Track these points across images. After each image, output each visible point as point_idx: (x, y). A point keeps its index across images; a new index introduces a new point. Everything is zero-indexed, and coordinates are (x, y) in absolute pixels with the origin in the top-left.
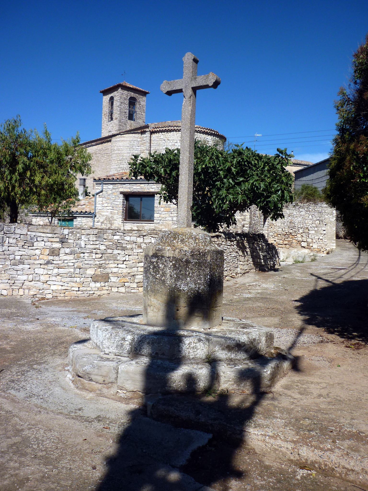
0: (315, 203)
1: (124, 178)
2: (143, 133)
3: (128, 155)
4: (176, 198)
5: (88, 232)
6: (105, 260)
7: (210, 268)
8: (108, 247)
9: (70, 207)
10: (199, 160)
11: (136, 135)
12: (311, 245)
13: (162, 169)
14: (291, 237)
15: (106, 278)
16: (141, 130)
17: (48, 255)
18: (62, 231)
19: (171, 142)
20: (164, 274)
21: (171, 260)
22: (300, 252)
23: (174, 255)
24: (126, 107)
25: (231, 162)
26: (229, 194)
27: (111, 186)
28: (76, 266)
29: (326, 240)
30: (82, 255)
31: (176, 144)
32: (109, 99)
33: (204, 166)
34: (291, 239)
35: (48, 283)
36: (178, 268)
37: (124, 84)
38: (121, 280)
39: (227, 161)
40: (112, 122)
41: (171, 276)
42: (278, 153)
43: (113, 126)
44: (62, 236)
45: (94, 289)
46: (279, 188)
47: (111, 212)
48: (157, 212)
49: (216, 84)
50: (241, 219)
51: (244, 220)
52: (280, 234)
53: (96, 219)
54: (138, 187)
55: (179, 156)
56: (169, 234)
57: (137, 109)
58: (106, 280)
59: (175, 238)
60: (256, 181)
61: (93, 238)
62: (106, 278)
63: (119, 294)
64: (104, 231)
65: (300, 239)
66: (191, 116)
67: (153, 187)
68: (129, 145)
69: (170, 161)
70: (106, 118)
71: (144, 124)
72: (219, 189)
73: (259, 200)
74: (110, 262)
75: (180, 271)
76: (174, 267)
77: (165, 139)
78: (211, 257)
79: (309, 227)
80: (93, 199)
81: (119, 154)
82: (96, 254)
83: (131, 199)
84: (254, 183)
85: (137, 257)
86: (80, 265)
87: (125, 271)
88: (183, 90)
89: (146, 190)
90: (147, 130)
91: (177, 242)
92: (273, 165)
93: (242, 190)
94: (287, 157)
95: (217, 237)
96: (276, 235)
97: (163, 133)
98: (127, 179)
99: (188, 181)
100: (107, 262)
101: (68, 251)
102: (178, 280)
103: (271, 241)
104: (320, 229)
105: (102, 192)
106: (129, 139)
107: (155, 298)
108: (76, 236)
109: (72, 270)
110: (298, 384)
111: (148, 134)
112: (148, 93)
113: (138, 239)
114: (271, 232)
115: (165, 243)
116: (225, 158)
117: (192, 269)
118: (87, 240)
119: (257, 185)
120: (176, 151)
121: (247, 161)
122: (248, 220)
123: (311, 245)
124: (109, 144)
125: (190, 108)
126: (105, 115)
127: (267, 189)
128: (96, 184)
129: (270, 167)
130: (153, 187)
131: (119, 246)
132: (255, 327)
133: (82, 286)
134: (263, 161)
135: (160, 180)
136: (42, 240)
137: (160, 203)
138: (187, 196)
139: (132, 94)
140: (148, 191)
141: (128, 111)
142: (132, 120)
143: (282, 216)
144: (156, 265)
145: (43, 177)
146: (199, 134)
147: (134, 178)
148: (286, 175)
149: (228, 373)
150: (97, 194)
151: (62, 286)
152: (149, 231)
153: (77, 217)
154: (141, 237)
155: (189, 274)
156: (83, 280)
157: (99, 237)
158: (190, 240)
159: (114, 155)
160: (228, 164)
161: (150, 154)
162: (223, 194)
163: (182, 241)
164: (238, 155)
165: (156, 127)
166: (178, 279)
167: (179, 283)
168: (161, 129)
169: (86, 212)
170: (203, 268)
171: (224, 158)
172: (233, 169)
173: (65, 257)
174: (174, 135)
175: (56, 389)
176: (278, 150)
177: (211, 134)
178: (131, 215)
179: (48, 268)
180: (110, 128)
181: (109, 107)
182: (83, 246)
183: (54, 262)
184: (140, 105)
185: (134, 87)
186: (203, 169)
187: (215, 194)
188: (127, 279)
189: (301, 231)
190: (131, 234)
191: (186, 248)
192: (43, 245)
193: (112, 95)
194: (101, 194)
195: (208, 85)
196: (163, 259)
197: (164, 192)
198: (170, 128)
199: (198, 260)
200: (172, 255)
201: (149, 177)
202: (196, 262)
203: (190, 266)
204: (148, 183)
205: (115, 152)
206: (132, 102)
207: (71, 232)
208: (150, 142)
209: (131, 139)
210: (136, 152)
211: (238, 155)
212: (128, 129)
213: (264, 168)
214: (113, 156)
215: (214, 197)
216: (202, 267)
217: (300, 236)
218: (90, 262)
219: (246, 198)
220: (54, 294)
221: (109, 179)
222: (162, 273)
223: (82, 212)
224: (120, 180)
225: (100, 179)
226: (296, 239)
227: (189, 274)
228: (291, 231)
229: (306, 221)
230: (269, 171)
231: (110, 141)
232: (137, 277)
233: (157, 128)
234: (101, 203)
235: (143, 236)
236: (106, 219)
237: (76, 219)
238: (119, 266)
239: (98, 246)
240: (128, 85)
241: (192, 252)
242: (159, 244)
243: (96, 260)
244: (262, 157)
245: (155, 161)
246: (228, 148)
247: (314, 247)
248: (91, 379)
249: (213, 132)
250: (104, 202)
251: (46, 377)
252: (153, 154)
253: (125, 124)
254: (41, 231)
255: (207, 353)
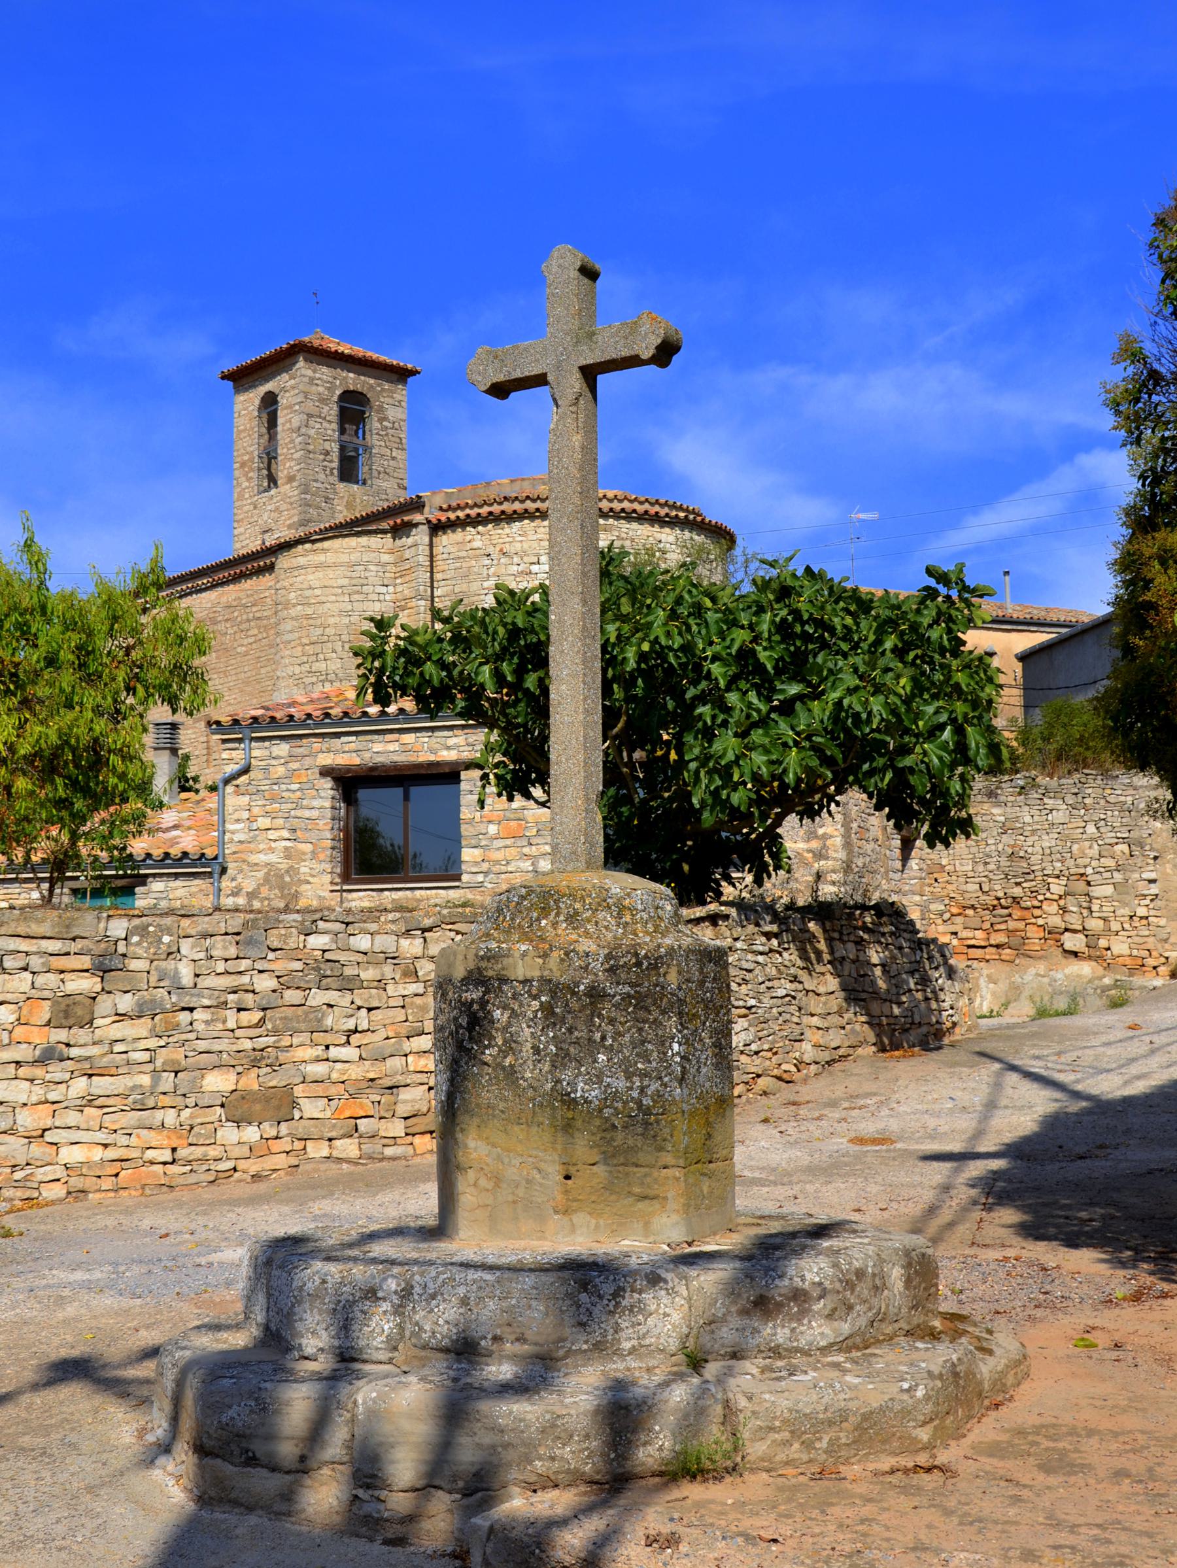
0: (1106, 774)
1: (336, 712)
2: (400, 531)
3: (346, 620)
4: (543, 779)
5: (204, 924)
6: (276, 1032)
7: (680, 1014)
8: (285, 982)
9: (124, 835)
10: (626, 628)
11: (374, 541)
12: (1103, 943)
13: (486, 669)
14: (1017, 914)
15: (281, 1106)
16: (395, 520)
17: (48, 1024)
18: (102, 925)
19: (516, 560)
20: (511, 1045)
21: (534, 991)
22: (1059, 976)
23: (546, 973)
24: (327, 431)
25: (751, 627)
26: (750, 750)
27: (282, 749)
28: (159, 1063)
29: (1163, 922)
30: (184, 1017)
31: (535, 568)
32: (257, 402)
33: (646, 647)
34: (1021, 925)
35: (49, 1137)
36: (563, 1021)
37: (316, 343)
38: (342, 1111)
39: (735, 624)
40: (273, 492)
41: (536, 1050)
42: (932, 582)
43: (277, 509)
44: (103, 945)
45: (236, 1152)
46: (943, 718)
47: (286, 848)
48: (473, 842)
49: (666, 352)
50: (809, 851)
51: (820, 855)
52: (973, 907)
53: (226, 883)
54: (392, 747)
55: (546, 614)
56: (523, 898)
57: (374, 440)
58: (282, 1114)
59: (545, 912)
60: (851, 691)
61: (223, 948)
62: (281, 1106)
63: (334, 1166)
64: (267, 919)
65: (1056, 921)
66: (581, 469)
67: (451, 742)
68: (345, 582)
69: (514, 633)
70: (249, 479)
71: (403, 497)
72: (709, 735)
73: (866, 767)
74: (296, 1041)
75: (570, 1030)
76: (546, 1018)
77: (490, 550)
78: (679, 973)
79: (1089, 871)
80: (212, 802)
81: (308, 617)
82: (239, 1010)
83: (363, 794)
84: (846, 702)
85: (400, 1015)
86: (175, 1056)
87: (355, 1072)
88: (550, 378)
89: (424, 757)
90: (417, 518)
91: (555, 925)
92: (914, 627)
93: (798, 734)
94: (966, 595)
95: (713, 919)
96: (955, 910)
97: (480, 528)
98: (346, 714)
99: (585, 700)
100: (286, 1041)
101: (126, 1003)
102: (564, 1065)
103: (927, 930)
104: (1136, 876)
105: (246, 770)
106: (344, 558)
107: (480, 1138)
108: (160, 941)
109: (145, 1080)
110: (1038, 1439)
111: (421, 535)
112: (414, 373)
113: (405, 943)
114: (936, 899)
115: (507, 932)
116: (728, 611)
117: (612, 1021)
118: (202, 955)
119: (858, 708)
120: (536, 597)
121: (811, 618)
122: (838, 853)
123: (1103, 943)
124: (266, 580)
125: (577, 439)
126: (243, 465)
127: (900, 720)
128: (224, 741)
129: (902, 640)
130: (455, 743)
131: (328, 972)
132: (863, 1231)
133: (185, 1142)
134: (876, 618)
135: (476, 713)
136: (21, 964)
137: (482, 803)
138: (581, 757)
139: (352, 380)
140: (432, 758)
141: (335, 447)
142: (357, 483)
143: (966, 826)
144: (481, 1014)
145: (22, 726)
146: (623, 524)
147: (374, 710)
148: (967, 666)
149: (767, 1396)
150: (227, 781)
151: (106, 1146)
152: (445, 912)
153: (147, 876)
154: (414, 937)
155: (603, 1038)
156: (191, 1117)
157: (250, 942)
158: (601, 915)
159: (289, 625)
160: (741, 636)
161: (436, 614)
162: (725, 750)
163: (573, 919)
164: (778, 600)
165: (454, 504)
166: (561, 1059)
167: (566, 1076)
168: (473, 512)
169: (185, 854)
170: (655, 1014)
171: (724, 612)
172: (763, 656)
173: (117, 1031)
174: (525, 534)
175: (117, 1510)
176: (929, 572)
177: (684, 524)
178: (367, 857)
179: (48, 1077)
180: (266, 518)
181: (261, 436)
182: (187, 979)
183: (74, 1052)
184: (385, 419)
185: (359, 351)
186: (642, 657)
187: (696, 751)
188: (366, 1104)
189: (1057, 888)
190: (373, 927)
191: (587, 945)
192: (25, 986)
193: (269, 386)
194: (243, 779)
195: (637, 356)
196: (505, 988)
197: (499, 757)
198: (507, 507)
199: (631, 985)
200: (536, 974)
201: (433, 702)
202: (629, 996)
203: (606, 1009)
204: (433, 729)
205: (293, 612)
206: (353, 410)
207: (136, 927)
208: (432, 566)
209: (355, 557)
210: (377, 606)
211: (778, 600)
212: (340, 518)
213: (878, 642)
214: (282, 627)
215: (693, 766)
216: (649, 1012)
217: (1054, 908)
218: (216, 1046)
219: (814, 763)
220: (72, 1181)
221: (273, 718)
222: (505, 1041)
223: (167, 855)
224: (325, 723)
225: (236, 722)
226: (1040, 922)
227: (603, 1038)
228: (1017, 892)
229: (1075, 847)
230: (899, 653)
231: (271, 568)
232: (404, 1095)
233: (454, 510)
234: (246, 815)
235: (424, 930)
236: (266, 880)
237: (144, 884)
238: (334, 1052)
239: (245, 979)
240: (333, 347)
241: (609, 957)
242: (488, 935)
243: (238, 1033)
244: (871, 601)
245: (457, 640)
246: (738, 576)
247: (1116, 949)
248: (254, 1458)
249: (682, 515)
250: (256, 811)
251: (73, 1475)
252: (446, 613)
253: (327, 500)
254: (21, 930)
255: (685, 1330)
